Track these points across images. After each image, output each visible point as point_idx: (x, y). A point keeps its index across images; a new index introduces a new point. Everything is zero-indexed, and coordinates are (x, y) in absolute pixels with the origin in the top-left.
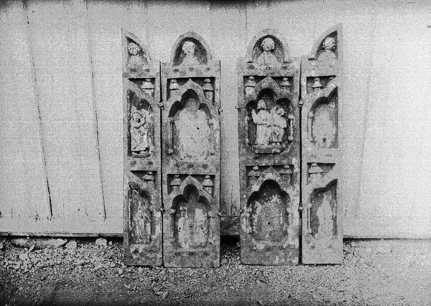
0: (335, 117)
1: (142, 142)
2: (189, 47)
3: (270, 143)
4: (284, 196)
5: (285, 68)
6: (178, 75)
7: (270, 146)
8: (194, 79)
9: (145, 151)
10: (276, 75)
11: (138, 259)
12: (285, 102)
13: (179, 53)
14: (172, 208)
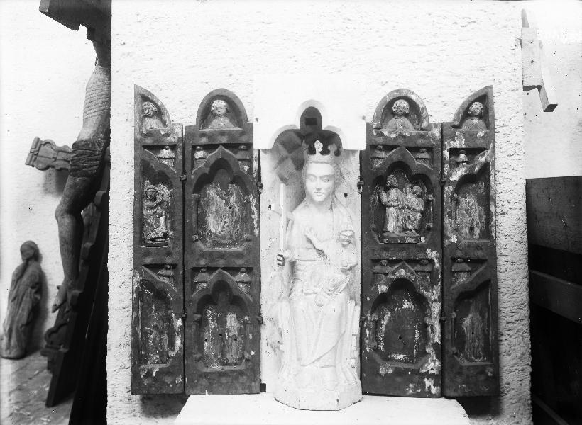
1: (160, 227)
2: (220, 105)
4: (421, 302)
6: (204, 140)
7: (403, 234)
8: (226, 145)
9: (161, 238)
10: (410, 145)
11: (150, 386)
12: (420, 179)
13: (206, 114)
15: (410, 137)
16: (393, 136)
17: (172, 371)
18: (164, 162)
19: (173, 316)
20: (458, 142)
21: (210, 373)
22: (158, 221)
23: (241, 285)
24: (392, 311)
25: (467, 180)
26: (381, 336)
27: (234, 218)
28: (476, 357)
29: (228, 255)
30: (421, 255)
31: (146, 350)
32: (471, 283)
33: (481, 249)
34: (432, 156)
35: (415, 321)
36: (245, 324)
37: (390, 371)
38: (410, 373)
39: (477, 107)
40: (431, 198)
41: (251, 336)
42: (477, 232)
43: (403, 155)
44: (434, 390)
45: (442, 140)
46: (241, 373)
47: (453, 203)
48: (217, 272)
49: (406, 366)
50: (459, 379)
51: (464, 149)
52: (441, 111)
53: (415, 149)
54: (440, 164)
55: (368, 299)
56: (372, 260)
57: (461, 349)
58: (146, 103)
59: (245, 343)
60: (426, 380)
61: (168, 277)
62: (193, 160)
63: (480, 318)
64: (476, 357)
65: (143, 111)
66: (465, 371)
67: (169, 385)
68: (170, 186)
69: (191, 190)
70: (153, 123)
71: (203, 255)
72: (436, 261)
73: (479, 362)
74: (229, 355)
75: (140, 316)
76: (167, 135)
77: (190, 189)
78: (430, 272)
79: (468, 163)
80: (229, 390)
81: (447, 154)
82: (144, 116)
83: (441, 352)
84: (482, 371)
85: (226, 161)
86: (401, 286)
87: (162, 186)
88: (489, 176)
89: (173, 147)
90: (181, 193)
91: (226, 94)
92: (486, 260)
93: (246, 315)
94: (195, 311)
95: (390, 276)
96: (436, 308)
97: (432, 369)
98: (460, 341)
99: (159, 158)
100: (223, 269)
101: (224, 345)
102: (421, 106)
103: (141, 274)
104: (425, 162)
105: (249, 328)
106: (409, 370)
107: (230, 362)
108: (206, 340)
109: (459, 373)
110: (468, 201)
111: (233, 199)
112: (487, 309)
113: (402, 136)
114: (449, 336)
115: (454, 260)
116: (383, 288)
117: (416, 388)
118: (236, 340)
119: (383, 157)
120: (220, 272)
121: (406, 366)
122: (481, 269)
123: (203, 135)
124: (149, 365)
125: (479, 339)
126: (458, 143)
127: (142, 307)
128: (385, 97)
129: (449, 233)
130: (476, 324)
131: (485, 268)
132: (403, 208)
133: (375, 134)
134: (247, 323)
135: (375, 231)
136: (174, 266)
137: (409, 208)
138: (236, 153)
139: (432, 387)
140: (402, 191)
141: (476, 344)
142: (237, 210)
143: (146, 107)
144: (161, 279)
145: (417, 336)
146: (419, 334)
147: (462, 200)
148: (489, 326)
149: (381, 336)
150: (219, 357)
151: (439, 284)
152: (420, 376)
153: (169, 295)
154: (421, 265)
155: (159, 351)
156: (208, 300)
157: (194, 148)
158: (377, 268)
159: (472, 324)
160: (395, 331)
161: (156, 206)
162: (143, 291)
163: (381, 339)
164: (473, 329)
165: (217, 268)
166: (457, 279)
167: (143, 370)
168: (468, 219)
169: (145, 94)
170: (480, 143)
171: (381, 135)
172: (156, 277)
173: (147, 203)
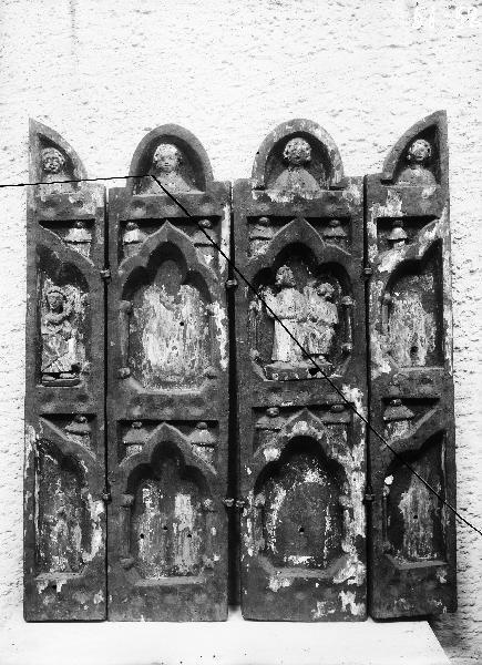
0: (437, 303)
1: (67, 355)
2: (167, 152)
3: (306, 355)
4: (334, 473)
5: (333, 200)
6: (139, 213)
8: (174, 221)
9: (70, 372)
10: (313, 214)
12: (330, 271)
13: (146, 167)
14: (127, 493)
15: (313, 202)
16: (285, 200)
17: (87, 584)
18: (77, 249)
19: (90, 496)
20: (390, 207)
21: (148, 588)
22: (63, 346)
23: (199, 449)
24: (287, 487)
25: (407, 270)
26: (272, 527)
27: (188, 341)
28: (421, 554)
29: (177, 400)
30: (334, 397)
31: (46, 549)
32: (414, 437)
33: (430, 381)
34: (350, 233)
35: (325, 503)
36: (204, 511)
37: (287, 584)
38: (317, 585)
39: (420, 147)
40: (348, 301)
41: (214, 531)
42: (422, 354)
43: (303, 232)
44: (356, 609)
45: (365, 205)
46: (197, 589)
47: (384, 307)
48: (159, 427)
49: (313, 574)
50: (395, 591)
51: (399, 218)
52: (360, 159)
53: (322, 222)
54: (362, 245)
55: (249, 472)
56: (253, 408)
57: (398, 543)
58: (48, 150)
59: (205, 541)
60: (342, 594)
61: (82, 434)
62: (122, 245)
63: (427, 493)
64: (421, 554)
65: (42, 164)
66: (404, 577)
67: (83, 606)
68: (85, 287)
69: (118, 294)
70: (57, 186)
71: (137, 400)
72: (358, 405)
73: (426, 562)
74: (178, 561)
75: (37, 496)
76: (79, 203)
77: (115, 293)
78: (346, 424)
79: (407, 241)
80: (177, 615)
81: (372, 228)
82: (44, 171)
83: (366, 549)
84: (430, 574)
85: (175, 246)
86: (300, 449)
87: (71, 288)
88: (441, 264)
89: (89, 224)
90: (102, 300)
91: (178, 134)
92: (438, 399)
93: (207, 496)
94: (124, 490)
95: (283, 433)
96: (357, 482)
97: (352, 578)
98: (396, 529)
99: (66, 242)
100: (169, 422)
101: (171, 544)
102: (330, 148)
103: (37, 430)
104: (338, 243)
105: (211, 518)
106: (315, 580)
107: (181, 570)
108: (142, 536)
109: (395, 582)
110: (410, 305)
111: (187, 309)
112: (439, 477)
113: (298, 199)
114: (378, 525)
115: (388, 402)
116: (272, 453)
117: (326, 608)
118: (190, 536)
119: (269, 236)
120: (163, 428)
121: (313, 574)
122: (429, 415)
123: (138, 204)
124: (52, 575)
125: (425, 526)
126: (392, 209)
127: (40, 481)
128: (271, 135)
129: (377, 358)
130: (421, 502)
131: (437, 413)
132: (304, 320)
133: (255, 198)
134: (208, 511)
135: (259, 361)
136: (91, 418)
137: (314, 320)
138: (191, 234)
139: (353, 605)
140: (302, 292)
141: (421, 533)
142: (193, 327)
143: (47, 156)
144: (70, 438)
145: (328, 524)
146: (332, 522)
147: (399, 303)
148: (440, 505)
149: (272, 527)
150: (163, 562)
151: (363, 442)
152: (331, 588)
153: (83, 462)
154: (334, 412)
155: (67, 552)
156: (145, 473)
157: (124, 226)
158: (263, 421)
159: (415, 502)
160: (293, 520)
161: (60, 323)
162: (41, 457)
163: (271, 532)
164: (416, 510)
165: (159, 422)
166: (391, 432)
167: (42, 582)
168: (407, 334)
169: (48, 134)
170: (424, 208)
171: (266, 199)
172: (62, 435)
173: (48, 316)
